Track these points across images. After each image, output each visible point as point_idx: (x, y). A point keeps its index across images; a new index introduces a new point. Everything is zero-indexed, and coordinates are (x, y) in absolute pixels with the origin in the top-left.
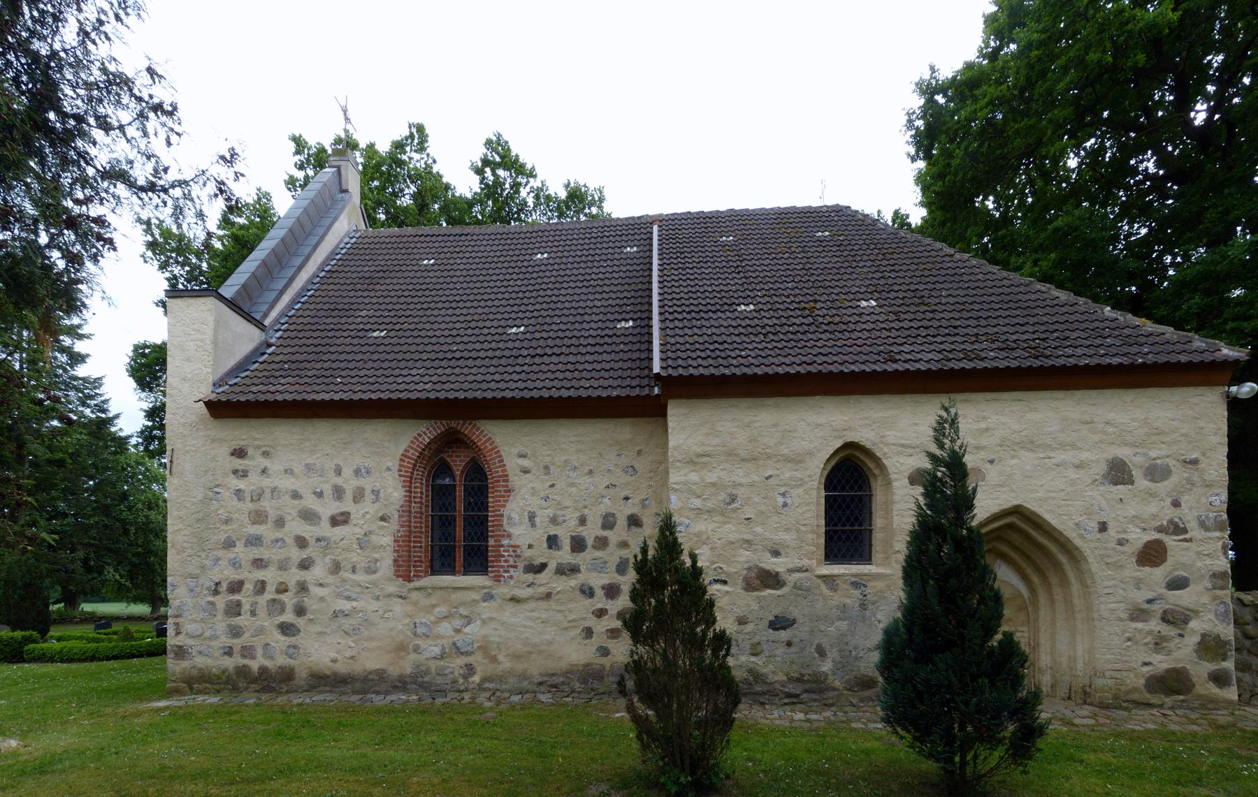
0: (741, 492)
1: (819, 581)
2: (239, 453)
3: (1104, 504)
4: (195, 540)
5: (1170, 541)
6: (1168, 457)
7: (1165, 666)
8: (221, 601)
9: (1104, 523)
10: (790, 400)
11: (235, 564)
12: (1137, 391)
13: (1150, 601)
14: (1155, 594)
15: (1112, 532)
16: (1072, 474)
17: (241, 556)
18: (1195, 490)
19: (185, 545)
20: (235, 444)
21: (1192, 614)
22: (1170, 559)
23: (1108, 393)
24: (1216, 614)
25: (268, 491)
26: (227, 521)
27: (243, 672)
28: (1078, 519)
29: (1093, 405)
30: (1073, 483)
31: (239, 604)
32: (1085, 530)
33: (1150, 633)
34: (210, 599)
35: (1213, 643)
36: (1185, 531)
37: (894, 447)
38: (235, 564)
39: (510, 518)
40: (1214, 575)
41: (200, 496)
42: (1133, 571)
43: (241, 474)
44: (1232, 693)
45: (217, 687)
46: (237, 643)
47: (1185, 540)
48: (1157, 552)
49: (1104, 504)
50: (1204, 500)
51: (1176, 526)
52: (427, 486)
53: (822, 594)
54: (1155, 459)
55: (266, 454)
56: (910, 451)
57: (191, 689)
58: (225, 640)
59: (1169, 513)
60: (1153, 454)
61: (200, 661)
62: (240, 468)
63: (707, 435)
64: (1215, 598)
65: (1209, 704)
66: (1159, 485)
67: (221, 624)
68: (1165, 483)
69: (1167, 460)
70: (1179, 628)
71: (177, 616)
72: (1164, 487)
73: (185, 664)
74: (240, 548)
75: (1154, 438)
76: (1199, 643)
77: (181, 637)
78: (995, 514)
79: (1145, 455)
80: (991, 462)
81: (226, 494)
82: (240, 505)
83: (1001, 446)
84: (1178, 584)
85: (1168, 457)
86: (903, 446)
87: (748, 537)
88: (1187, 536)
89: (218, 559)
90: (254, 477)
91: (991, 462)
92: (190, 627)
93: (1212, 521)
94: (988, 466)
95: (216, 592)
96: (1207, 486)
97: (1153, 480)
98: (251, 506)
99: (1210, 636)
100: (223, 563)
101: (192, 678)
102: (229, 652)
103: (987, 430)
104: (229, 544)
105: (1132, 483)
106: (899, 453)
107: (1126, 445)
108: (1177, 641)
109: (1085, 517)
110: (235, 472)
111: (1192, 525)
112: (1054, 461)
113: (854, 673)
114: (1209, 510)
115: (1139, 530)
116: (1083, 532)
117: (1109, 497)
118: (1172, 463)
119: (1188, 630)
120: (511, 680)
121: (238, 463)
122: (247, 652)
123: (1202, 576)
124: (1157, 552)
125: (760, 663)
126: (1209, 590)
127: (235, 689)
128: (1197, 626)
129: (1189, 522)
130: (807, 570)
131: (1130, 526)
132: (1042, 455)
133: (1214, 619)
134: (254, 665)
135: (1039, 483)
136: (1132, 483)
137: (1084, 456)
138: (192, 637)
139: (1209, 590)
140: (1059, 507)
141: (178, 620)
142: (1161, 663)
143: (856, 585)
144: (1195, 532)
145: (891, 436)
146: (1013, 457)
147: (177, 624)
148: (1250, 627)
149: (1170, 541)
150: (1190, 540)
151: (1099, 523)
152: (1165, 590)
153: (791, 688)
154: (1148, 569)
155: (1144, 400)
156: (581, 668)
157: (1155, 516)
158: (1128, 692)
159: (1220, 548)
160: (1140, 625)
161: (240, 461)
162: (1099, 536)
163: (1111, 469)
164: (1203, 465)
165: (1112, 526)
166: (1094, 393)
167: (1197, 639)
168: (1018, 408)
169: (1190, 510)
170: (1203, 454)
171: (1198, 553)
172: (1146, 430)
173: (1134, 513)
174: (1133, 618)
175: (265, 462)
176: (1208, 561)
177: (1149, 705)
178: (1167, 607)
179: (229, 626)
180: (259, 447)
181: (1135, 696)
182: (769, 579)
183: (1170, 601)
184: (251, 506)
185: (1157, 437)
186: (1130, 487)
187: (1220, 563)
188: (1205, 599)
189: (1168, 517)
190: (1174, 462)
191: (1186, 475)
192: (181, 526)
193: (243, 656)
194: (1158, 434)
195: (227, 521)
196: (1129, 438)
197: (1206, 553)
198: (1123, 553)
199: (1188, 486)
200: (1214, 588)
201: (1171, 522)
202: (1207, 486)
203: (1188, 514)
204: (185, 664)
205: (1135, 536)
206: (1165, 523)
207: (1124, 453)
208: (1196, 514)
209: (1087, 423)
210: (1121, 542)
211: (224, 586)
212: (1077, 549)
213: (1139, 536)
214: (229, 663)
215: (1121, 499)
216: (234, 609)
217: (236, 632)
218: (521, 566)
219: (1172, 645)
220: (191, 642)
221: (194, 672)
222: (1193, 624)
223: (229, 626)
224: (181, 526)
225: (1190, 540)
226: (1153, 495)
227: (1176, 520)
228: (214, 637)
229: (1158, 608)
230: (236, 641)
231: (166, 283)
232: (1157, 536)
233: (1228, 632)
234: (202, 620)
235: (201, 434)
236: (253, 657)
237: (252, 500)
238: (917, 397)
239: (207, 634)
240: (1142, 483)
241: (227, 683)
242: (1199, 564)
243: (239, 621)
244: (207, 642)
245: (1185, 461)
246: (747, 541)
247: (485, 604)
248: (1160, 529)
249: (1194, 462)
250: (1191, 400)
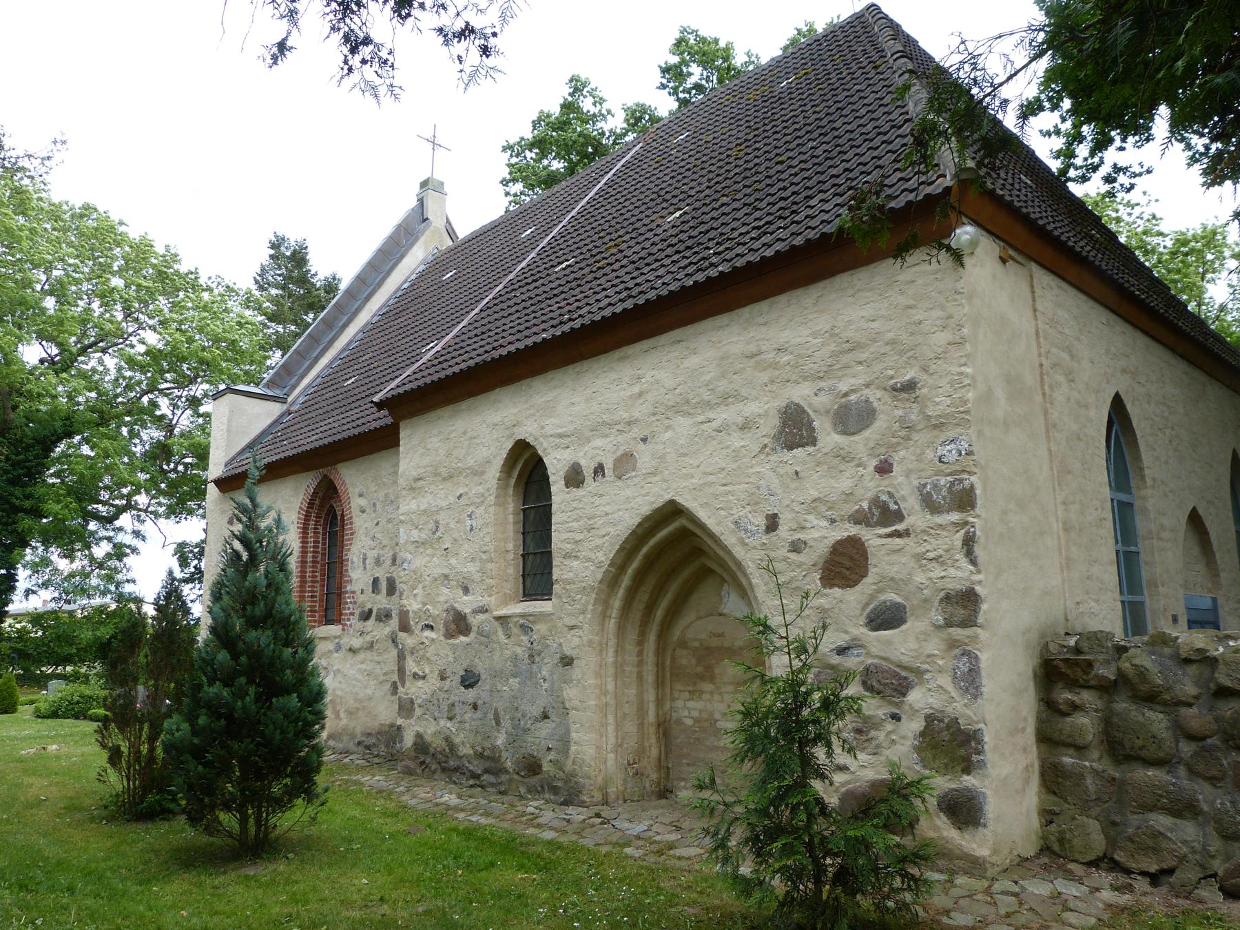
0: (442, 517)
1: (496, 624)
3: (775, 484)
5: (873, 538)
6: (867, 386)
7: (870, 775)
9: (775, 516)
10: (586, 364)
12: (821, 285)
14: (847, 637)
15: (783, 531)
16: (736, 441)
18: (915, 437)
21: (912, 677)
22: (872, 571)
23: (783, 298)
24: (955, 677)
28: (738, 513)
29: (765, 324)
30: (736, 455)
32: (746, 530)
35: (946, 736)
36: (899, 516)
37: (551, 439)
39: (353, 563)
40: (947, 599)
47: (897, 534)
48: (852, 559)
49: (775, 484)
50: (930, 454)
51: (884, 508)
52: (324, 534)
53: (498, 642)
54: (846, 395)
56: (566, 441)
59: (872, 486)
60: (843, 387)
63: (422, 455)
64: (952, 644)
66: (856, 438)
68: (867, 433)
69: (867, 392)
70: (891, 703)
72: (860, 443)
75: (845, 359)
76: (922, 734)
78: (647, 519)
79: (832, 390)
80: (644, 440)
83: (654, 414)
85: (867, 386)
86: (561, 436)
87: (446, 571)
88: (900, 527)
91: (644, 440)
93: (944, 492)
94: (641, 446)
96: (935, 427)
97: (845, 433)
99: (941, 721)
103: (640, 395)
105: (813, 441)
106: (557, 447)
107: (805, 379)
108: (889, 727)
109: (748, 508)
111: (911, 504)
112: (714, 425)
113: (523, 751)
114: (938, 473)
115: (825, 523)
116: (742, 534)
117: (782, 471)
118: (873, 395)
119: (906, 707)
120: (345, 738)
123: (925, 601)
124: (852, 559)
125: (454, 730)
126: (939, 627)
129: (904, 498)
130: (486, 611)
131: (811, 517)
132: (700, 419)
133: (950, 687)
135: (696, 463)
136: (813, 441)
137: (752, 408)
139: (939, 627)
140: (716, 496)
143: (526, 629)
144: (917, 518)
145: (552, 425)
146: (668, 428)
148: (1193, 711)
149: (873, 538)
150: (906, 534)
151: (768, 517)
152: (864, 630)
153: (478, 767)
154: (837, 592)
155: (833, 296)
156: (387, 729)
157: (848, 496)
159: (959, 543)
162: (765, 539)
163: (784, 424)
164: (925, 391)
166: (764, 305)
167: (917, 725)
168: (676, 354)
169: (907, 476)
170: (925, 369)
171: (919, 557)
172: (832, 347)
173: (815, 494)
176: (937, 572)
178: (869, 661)
182: (458, 624)
183: (874, 651)
185: (850, 356)
186: (810, 449)
187: (959, 574)
188: (934, 646)
189: (870, 495)
190: (879, 394)
191: (900, 412)
194: (851, 350)
196: (809, 366)
197: (931, 555)
198: (800, 565)
199: (903, 433)
200: (949, 624)
201: (876, 502)
202: (935, 427)
205: (817, 535)
206: (865, 505)
207: (801, 393)
208: (916, 483)
209: (753, 356)
210: (796, 547)
212: (739, 564)
213: (824, 533)
215: (797, 473)
218: (357, 612)
219: (880, 735)
222: (916, 697)
225: (906, 534)
226: (845, 457)
227: (884, 498)
232: (853, 530)
238: (578, 367)
240: (829, 438)
242: (920, 578)
245: (895, 389)
246: (446, 577)
247: (336, 655)
248: (860, 518)
249: (910, 386)
250: (900, 278)
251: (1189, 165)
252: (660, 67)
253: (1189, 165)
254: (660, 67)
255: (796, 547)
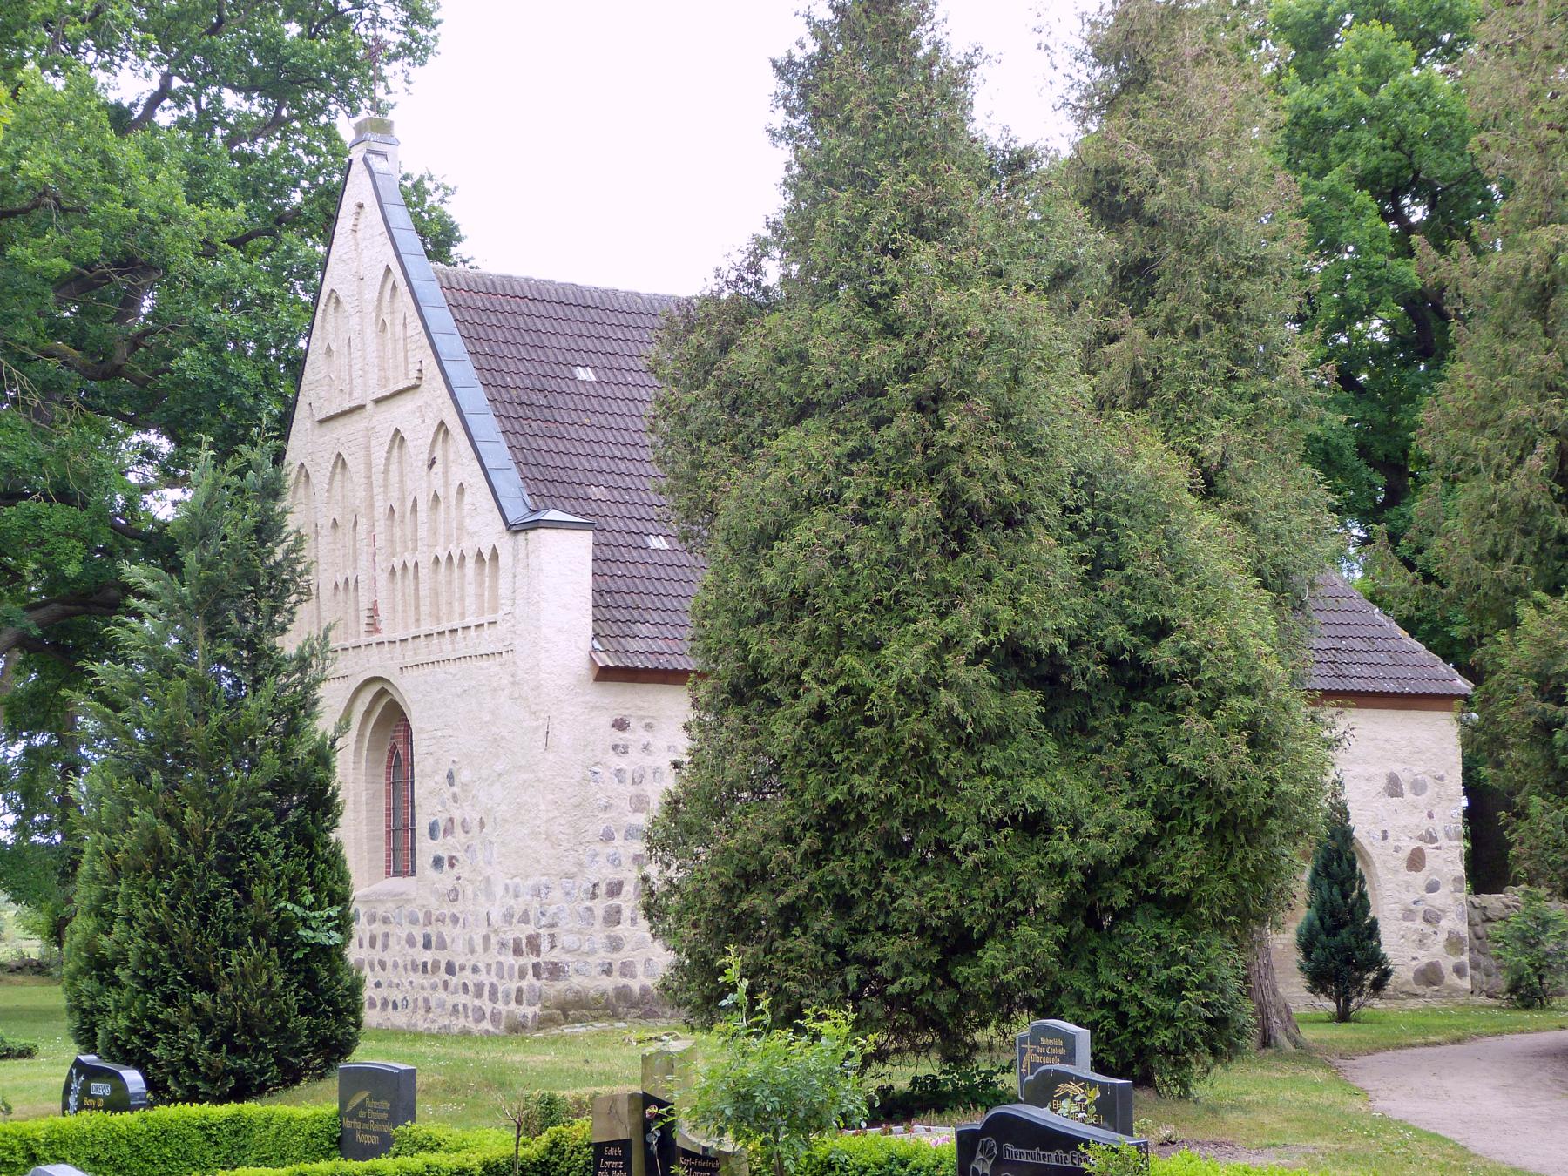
2: (620, 725)
4: (571, 831)
8: (600, 906)
11: (615, 861)
13: (1415, 903)
15: (1390, 839)
17: (621, 850)
19: (562, 837)
20: (618, 714)
25: (649, 771)
26: (606, 808)
27: (623, 994)
31: (619, 911)
33: (1416, 930)
34: (588, 904)
38: (615, 861)
41: (578, 777)
42: (1406, 876)
43: (620, 749)
44: (1466, 983)
45: (594, 1013)
46: (617, 958)
55: (648, 727)
57: (566, 1016)
58: (603, 955)
59: (1427, 824)
61: (576, 982)
62: (621, 743)
65: (1454, 991)
67: (599, 934)
71: (552, 926)
73: (560, 985)
74: (619, 840)
77: (556, 951)
81: (605, 774)
82: (621, 788)
84: (1432, 887)
89: (596, 855)
90: (634, 754)
92: (566, 940)
95: (594, 896)
98: (633, 790)
100: (601, 859)
101: (567, 1003)
102: (608, 971)
104: (608, 837)
110: (615, 747)
111: (1440, 835)
118: (1428, 778)
121: (619, 737)
122: (627, 969)
127: (615, 1016)
128: (1445, 924)
134: (635, 985)
137: (1373, 770)
138: (568, 951)
141: (554, 930)
142: (1424, 958)
144: (1443, 842)
147: (552, 936)
158: (1403, 984)
160: (1409, 924)
161: (621, 734)
165: (1390, 833)
167: (1445, 936)
174: (1405, 918)
175: (646, 737)
177: (1416, 995)
179: (609, 937)
180: (643, 718)
181: (1407, 988)
184: (633, 790)
192: (556, 813)
193: (623, 974)
195: (606, 808)
203: (1438, 827)
204: (560, 985)
207: (1397, 768)
211: (603, 889)
214: (609, 984)
216: (613, 917)
217: (615, 944)
219: (1429, 941)
220: (566, 958)
221: (570, 996)
222: (1443, 923)
223: (609, 937)
224: (556, 813)
228: (592, 952)
229: (1420, 908)
230: (616, 956)
231: (974, 115)
232: (1420, 844)
233: (1464, 930)
234: (579, 932)
235: (580, 699)
236: (633, 976)
237: (634, 783)
239: (586, 947)
240: (1409, 796)
241: (605, 1008)
243: (619, 930)
244: (585, 958)
248: (1421, 838)
249: (1441, 778)
251: (440, 22)
252: (774, 62)
253: (440, 22)
254: (774, 62)
255: (1397, 849)
